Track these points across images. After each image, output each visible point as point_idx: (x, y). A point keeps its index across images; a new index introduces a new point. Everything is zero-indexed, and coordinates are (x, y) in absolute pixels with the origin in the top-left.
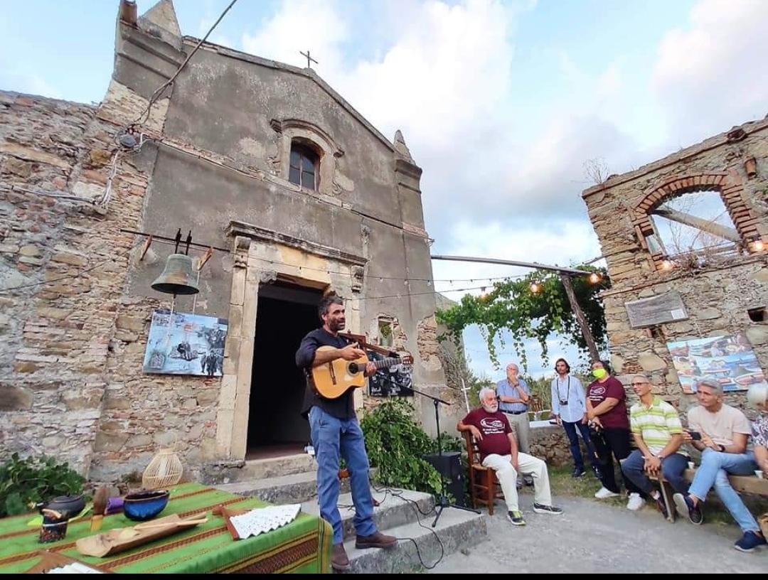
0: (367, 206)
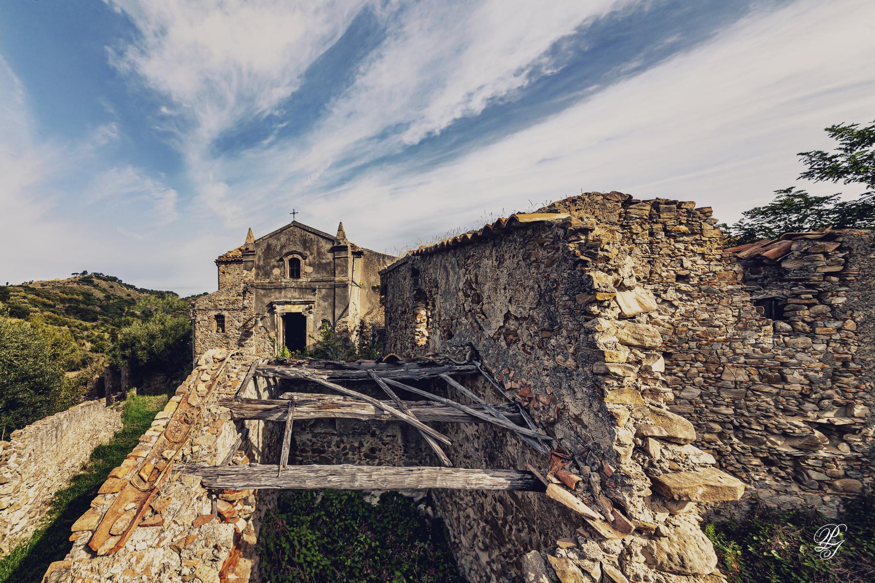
0: (319, 277)
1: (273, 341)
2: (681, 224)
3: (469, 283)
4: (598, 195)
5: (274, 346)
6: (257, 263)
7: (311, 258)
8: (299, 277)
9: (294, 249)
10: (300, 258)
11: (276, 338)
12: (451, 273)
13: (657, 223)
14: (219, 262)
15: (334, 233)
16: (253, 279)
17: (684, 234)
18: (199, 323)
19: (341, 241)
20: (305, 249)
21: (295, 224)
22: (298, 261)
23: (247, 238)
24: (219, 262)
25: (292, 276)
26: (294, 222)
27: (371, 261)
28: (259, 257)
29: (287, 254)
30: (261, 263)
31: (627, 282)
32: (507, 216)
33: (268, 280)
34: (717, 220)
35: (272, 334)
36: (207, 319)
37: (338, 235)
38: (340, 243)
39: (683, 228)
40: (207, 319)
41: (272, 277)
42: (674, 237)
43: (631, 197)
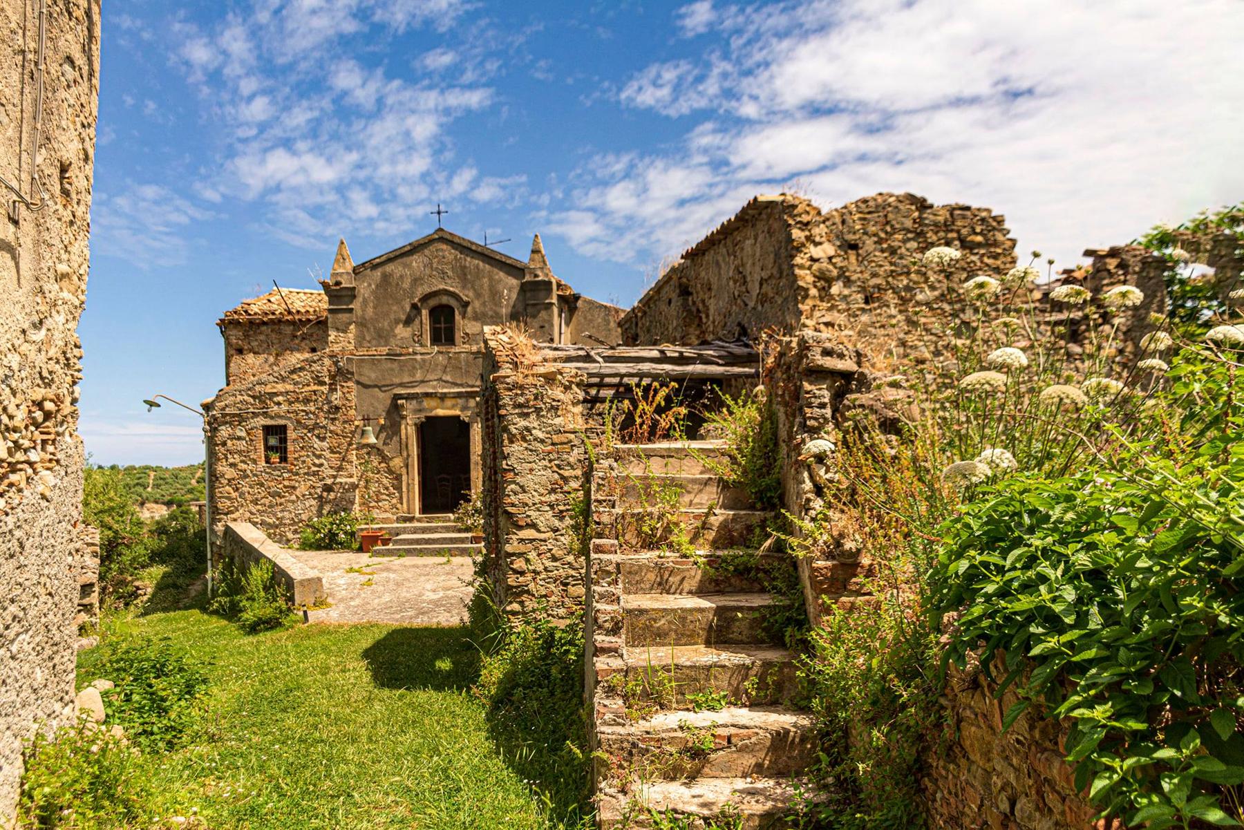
1: (398, 478)
2: (976, 234)
3: (737, 268)
4: (891, 196)
5: (399, 488)
6: (360, 313)
7: (477, 304)
8: (451, 341)
9: (442, 287)
10: (453, 303)
11: (404, 470)
12: (723, 265)
13: (952, 231)
14: (226, 325)
15: (522, 256)
16: (351, 347)
17: (979, 245)
18: (224, 444)
19: (539, 273)
20: (464, 287)
21: (442, 237)
22: (450, 310)
23: (337, 261)
24: (226, 325)
25: (436, 340)
26: (441, 230)
27: (591, 321)
28: (365, 300)
29: (426, 298)
30: (370, 311)
31: (818, 239)
32: (752, 198)
33: (385, 350)
34: (1008, 232)
35: (397, 462)
36: (243, 434)
37: (532, 260)
38: (536, 276)
39: (979, 239)
40: (243, 434)
41: (392, 341)
42: (971, 249)
43: (925, 200)
